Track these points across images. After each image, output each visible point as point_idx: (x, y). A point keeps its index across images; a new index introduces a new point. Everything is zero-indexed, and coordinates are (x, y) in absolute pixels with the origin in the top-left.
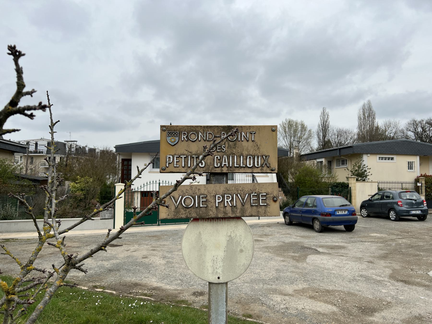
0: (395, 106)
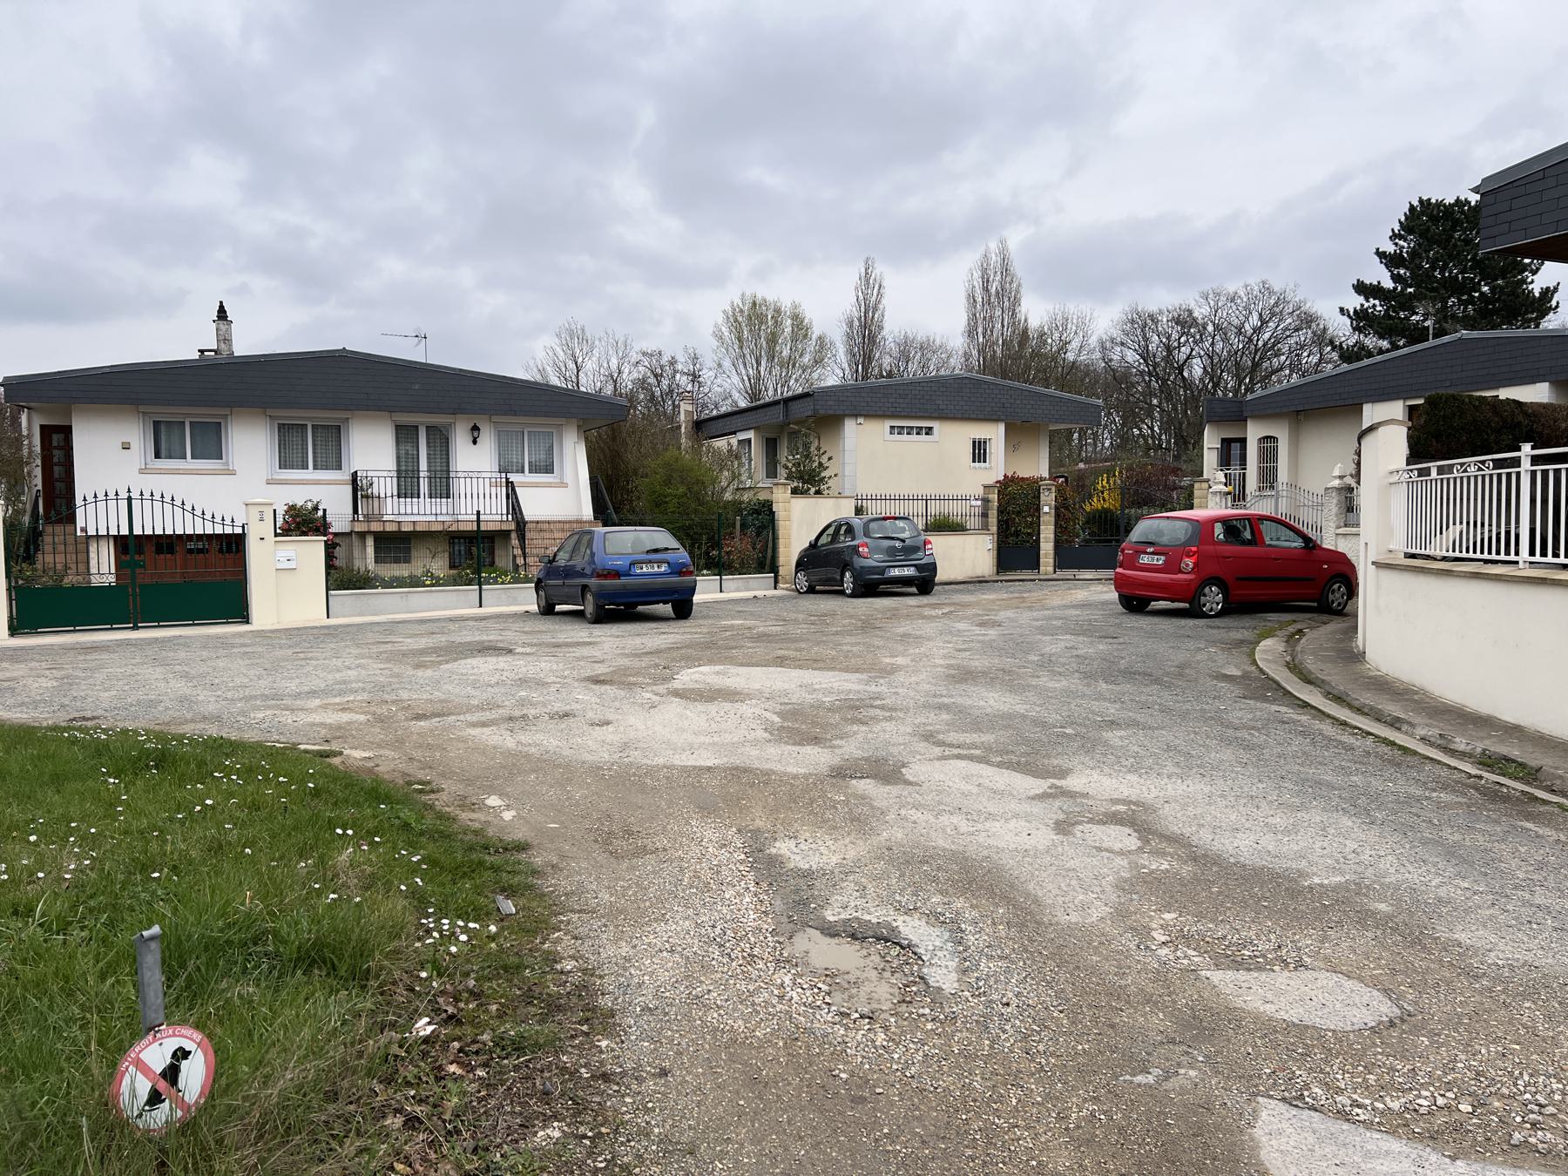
0: (1082, 266)
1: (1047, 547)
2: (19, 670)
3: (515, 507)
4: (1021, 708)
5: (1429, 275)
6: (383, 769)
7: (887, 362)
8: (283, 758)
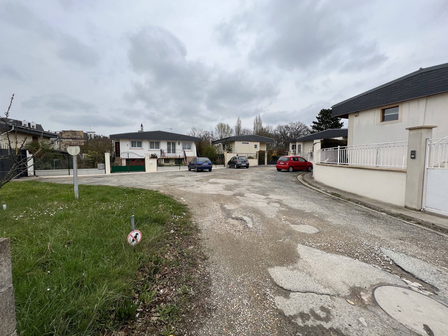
0: (272, 119)
1: (266, 161)
2: (112, 178)
3: (185, 155)
4: (262, 186)
5: (324, 121)
6: (166, 193)
7: (241, 133)
8: (151, 191)
